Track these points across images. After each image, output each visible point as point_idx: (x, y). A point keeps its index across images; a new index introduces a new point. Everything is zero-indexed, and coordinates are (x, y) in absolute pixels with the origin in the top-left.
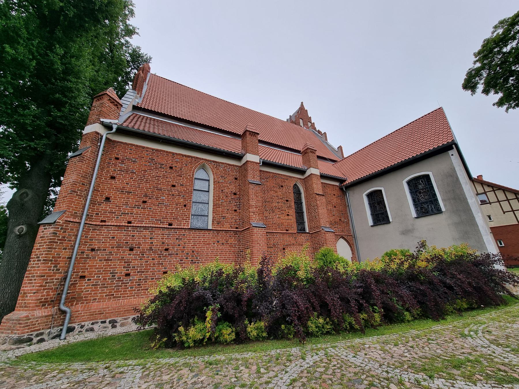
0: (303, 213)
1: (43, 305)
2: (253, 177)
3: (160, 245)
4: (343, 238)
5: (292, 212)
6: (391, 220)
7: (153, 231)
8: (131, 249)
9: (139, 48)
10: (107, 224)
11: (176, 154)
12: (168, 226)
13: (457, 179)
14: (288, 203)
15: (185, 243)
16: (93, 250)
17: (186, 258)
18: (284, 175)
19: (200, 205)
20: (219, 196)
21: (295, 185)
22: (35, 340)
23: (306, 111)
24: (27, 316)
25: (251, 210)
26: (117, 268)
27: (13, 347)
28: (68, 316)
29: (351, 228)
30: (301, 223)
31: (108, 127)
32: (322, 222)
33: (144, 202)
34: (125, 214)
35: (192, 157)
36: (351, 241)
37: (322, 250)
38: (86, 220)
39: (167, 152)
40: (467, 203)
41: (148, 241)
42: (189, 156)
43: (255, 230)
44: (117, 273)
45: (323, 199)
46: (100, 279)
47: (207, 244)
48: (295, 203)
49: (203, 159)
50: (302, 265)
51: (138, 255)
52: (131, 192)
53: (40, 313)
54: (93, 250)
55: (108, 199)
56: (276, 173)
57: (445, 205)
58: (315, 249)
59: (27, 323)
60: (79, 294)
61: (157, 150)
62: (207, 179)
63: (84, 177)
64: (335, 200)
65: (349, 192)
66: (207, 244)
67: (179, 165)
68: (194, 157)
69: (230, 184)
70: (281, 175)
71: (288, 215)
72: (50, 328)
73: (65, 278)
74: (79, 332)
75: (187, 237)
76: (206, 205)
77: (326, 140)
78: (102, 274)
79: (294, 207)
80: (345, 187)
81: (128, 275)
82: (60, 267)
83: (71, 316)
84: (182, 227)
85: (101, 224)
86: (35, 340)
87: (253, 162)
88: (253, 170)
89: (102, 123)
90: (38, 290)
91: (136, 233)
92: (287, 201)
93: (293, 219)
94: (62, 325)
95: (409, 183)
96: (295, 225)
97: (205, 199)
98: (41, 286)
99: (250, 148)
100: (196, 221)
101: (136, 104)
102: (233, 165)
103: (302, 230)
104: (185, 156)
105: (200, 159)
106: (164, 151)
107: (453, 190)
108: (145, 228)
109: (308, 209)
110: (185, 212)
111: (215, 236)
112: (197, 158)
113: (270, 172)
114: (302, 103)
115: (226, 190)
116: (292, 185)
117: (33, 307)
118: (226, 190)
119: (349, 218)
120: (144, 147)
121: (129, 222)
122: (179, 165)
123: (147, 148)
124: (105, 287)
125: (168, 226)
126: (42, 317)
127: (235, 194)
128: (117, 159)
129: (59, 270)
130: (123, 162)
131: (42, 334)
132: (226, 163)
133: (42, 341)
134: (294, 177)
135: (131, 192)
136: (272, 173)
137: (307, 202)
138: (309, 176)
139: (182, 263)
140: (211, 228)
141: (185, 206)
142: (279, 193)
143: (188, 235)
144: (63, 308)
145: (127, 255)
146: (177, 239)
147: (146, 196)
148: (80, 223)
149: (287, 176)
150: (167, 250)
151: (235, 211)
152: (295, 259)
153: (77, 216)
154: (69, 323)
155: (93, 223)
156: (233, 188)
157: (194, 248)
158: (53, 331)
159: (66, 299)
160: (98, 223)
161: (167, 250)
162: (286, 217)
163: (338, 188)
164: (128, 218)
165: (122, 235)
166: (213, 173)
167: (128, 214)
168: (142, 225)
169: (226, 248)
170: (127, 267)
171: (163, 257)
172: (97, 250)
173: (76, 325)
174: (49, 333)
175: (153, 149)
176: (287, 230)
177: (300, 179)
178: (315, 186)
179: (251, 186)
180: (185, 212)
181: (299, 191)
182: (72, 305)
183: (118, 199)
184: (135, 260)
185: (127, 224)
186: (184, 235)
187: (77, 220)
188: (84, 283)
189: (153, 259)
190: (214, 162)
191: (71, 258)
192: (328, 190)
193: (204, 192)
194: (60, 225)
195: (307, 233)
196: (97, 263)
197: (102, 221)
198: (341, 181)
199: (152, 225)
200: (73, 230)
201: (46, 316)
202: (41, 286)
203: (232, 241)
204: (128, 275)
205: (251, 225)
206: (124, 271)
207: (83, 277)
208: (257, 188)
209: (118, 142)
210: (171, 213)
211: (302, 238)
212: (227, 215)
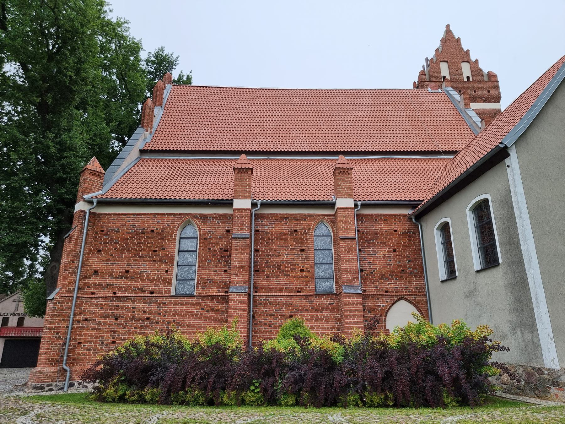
1: (51, 364)
3: (142, 314)
4: (406, 299)
7: (135, 301)
8: (116, 319)
9: (162, 49)
10: (96, 296)
11: (157, 214)
12: (149, 295)
13: (512, 208)
14: (304, 253)
15: (165, 312)
16: (86, 320)
18: (299, 214)
19: (187, 268)
20: (205, 257)
22: (47, 389)
23: (458, 40)
24: (40, 371)
25: (233, 272)
26: (104, 336)
27: (33, 391)
28: (68, 373)
31: (90, 202)
33: (127, 272)
34: (111, 285)
35: (174, 214)
38: (77, 294)
39: (148, 214)
40: (520, 250)
41: (131, 310)
42: (171, 214)
44: (105, 340)
46: (92, 346)
49: (187, 214)
51: (122, 324)
52: (115, 263)
53: (49, 369)
54: (86, 320)
55: (96, 272)
56: (286, 214)
57: (501, 253)
59: (41, 376)
60: (78, 357)
61: (138, 214)
63: (74, 256)
67: (160, 227)
68: (177, 214)
69: (220, 239)
70: (296, 215)
72: (56, 381)
73: (65, 344)
74: (78, 387)
76: (193, 267)
78: (93, 341)
81: (114, 342)
82: (61, 334)
83: (71, 373)
84: (163, 295)
85: (91, 296)
86: (47, 389)
87: (242, 210)
88: (241, 220)
89: (85, 200)
90: (46, 352)
91: (120, 304)
92: (302, 250)
94: (65, 381)
97: (192, 260)
98: (48, 349)
100: (182, 286)
101: (142, 148)
102: (225, 215)
104: (167, 214)
105: (184, 215)
106: (145, 214)
108: (128, 298)
110: (167, 278)
111: (199, 303)
112: (180, 214)
113: (277, 215)
114: (448, 26)
115: (215, 248)
117: (44, 364)
118: (215, 248)
120: (125, 214)
121: (115, 293)
122: (160, 227)
123: (129, 214)
124: (96, 353)
125: (149, 295)
126: (50, 372)
128: (102, 231)
129: (60, 337)
130: (107, 234)
131: (51, 385)
133: (51, 390)
134: (317, 215)
135: (115, 263)
136: (280, 214)
139: (162, 332)
141: (167, 271)
142: (290, 241)
143: (169, 303)
144: (65, 367)
145: (114, 324)
146: (158, 307)
147: (128, 265)
148: (73, 297)
149: (305, 215)
150: (148, 319)
153: (71, 291)
154: (69, 380)
155: (85, 296)
157: (175, 316)
158: (59, 384)
159: (67, 360)
160: (89, 296)
161: (148, 319)
162: (299, 274)
164: (113, 289)
165: (108, 305)
167: (113, 285)
168: (125, 295)
170: (113, 336)
171: (145, 326)
172: (90, 320)
173: (75, 382)
174: (56, 386)
175: (134, 214)
176: (298, 292)
177: (328, 215)
180: (167, 278)
182: (73, 366)
183: (105, 272)
184: (120, 328)
185: (112, 295)
186: (165, 303)
187: (71, 295)
188: (81, 347)
189: (135, 328)
190: (200, 215)
191: (68, 327)
193: (191, 253)
194: (58, 301)
196: (89, 331)
197: (92, 294)
198: (413, 206)
199: (134, 295)
200: (68, 303)
201: (53, 372)
202: (48, 349)
204: (114, 342)
206: (111, 339)
207: (80, 343)
209: (103, 214)
210: (153, 281)
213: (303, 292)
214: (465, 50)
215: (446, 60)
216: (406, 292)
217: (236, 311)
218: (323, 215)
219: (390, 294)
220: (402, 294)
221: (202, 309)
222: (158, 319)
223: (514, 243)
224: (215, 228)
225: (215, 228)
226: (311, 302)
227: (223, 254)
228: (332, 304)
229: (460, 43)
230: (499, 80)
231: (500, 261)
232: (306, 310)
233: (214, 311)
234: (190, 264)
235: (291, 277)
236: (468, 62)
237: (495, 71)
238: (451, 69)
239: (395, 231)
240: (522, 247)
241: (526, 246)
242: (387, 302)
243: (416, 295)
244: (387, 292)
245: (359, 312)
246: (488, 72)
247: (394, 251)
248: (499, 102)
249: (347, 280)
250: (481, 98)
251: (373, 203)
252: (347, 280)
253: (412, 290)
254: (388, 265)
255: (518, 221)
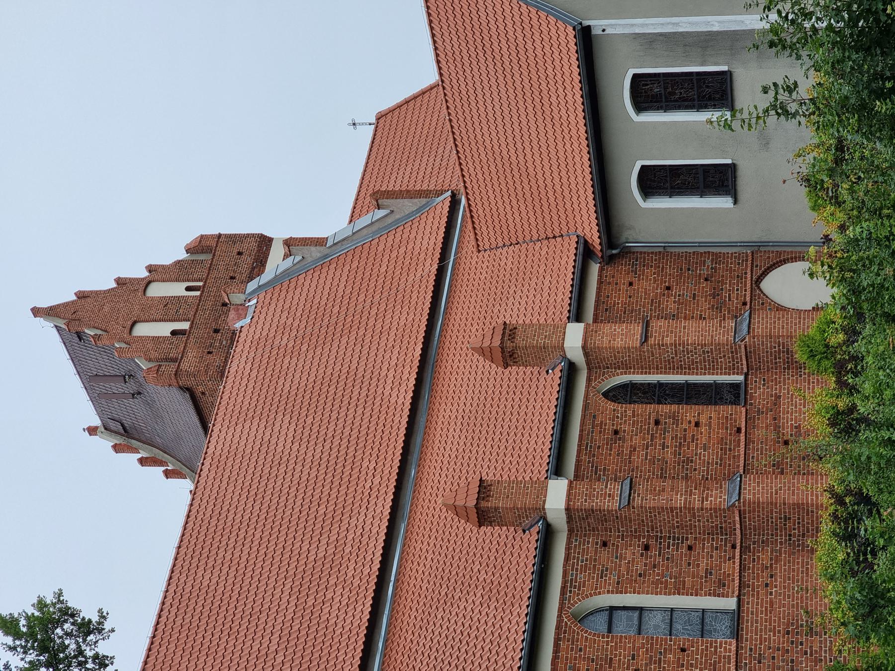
0: (688, 384)
2: (609, 497)
5: (689, 412)
6: (729, 161)
13: (661, 34)
14: (662, 421)
15: (770, 648)
17: (802, 644)
20: (657, 583)
21: (606, 395)
25: (697, 505)
29: (730, 250)
30: (717, 393)
32: (723, 339)
36: (773, 256)
37: (800, 356)
43: (747, 496)
45: (657, 325)
47: (772, 606)
48: (659, 403)
49: (559, 616)
50: (830, 401)
56: (579, 446)
57: (716, 64)
58: (792, 365)
62: (604, 616)
64: (648, 285)
65: (623, 239)
66: (772, 606)
68: (557, 634)
70: (581, 431)
71: (697, 424)
75: (756, 645)
76: (675, 616)
77: (320, 242)
79: (674, 407)
80: (610, 246)
92: (657, 423)
93: (709, 414)
95: (639, 107)
96: (726, 410)
99: (529, 502)
102: (568, 549)
103: (734, 394)
107: (685, 45)
109: (680, 369)
111: (753, 590)
112: (558, 627)
113: (578, 461)
114: (36, 312)
115: (639, 567)
116: (611, 405)
119: (702, 250)
127: (647, 548)
132: (565, 566)
136: (578, 456)
137: (658, 370)
138: (586, 354)
139: (811, 652)
140: (735, 599)
142: (636, 440)
143: (751, 643)
146: (760, 662)
151: (690, 548)
152: (819, 413)
156: (631, 552)
163: (609, 270)
166: (595, 594)
169: (780, 570)
176: (739, 430)
177: (589, 380)
178: (619, 343)
179: (637, 502)
181: (624, 387)
186: (751, 650)
192: (619, 299)
195: (746, 379)
203: (765, 557)
205: (733, 505)
208: (641, 488)
211: (759, 393)
212: (703, 565)
213: (740, 424)
214: (114, 285)
215: (130, 323)
216: (746, 278)
217: (776, 491)
218: (588, 387)
219: (748, 299)
220: (749, 282)
221: (767, 585)
222: (783, 661)
223: (706, 42)
224: (595, 566)
225: (595, 566)
226: (759, 412)
227: (654, 552)
228: (764, 380)
229: (92, 292)
230: (216, 232)
231: (725, 68)
232: (775, 419)
233: (771, 564)
234: (668, 621)
235: (709, 442)
236: (149, 283)
237: (191, 237)
238: (159, 317)
239: (631, 284)
240: (715, 29)
241: (716, 24)
242: (763, 304)
243: (752, 263)
244: (745, 304)
245: (783, 317)
246: (187, 252)
247: (668, 288)
248: (270, 240)
249: (724, 336)
250: (253, 269)
251: (574, 304)
252: (724, 336)
253: (742, 270)
254: (694, 299)
255: (681, 30)
